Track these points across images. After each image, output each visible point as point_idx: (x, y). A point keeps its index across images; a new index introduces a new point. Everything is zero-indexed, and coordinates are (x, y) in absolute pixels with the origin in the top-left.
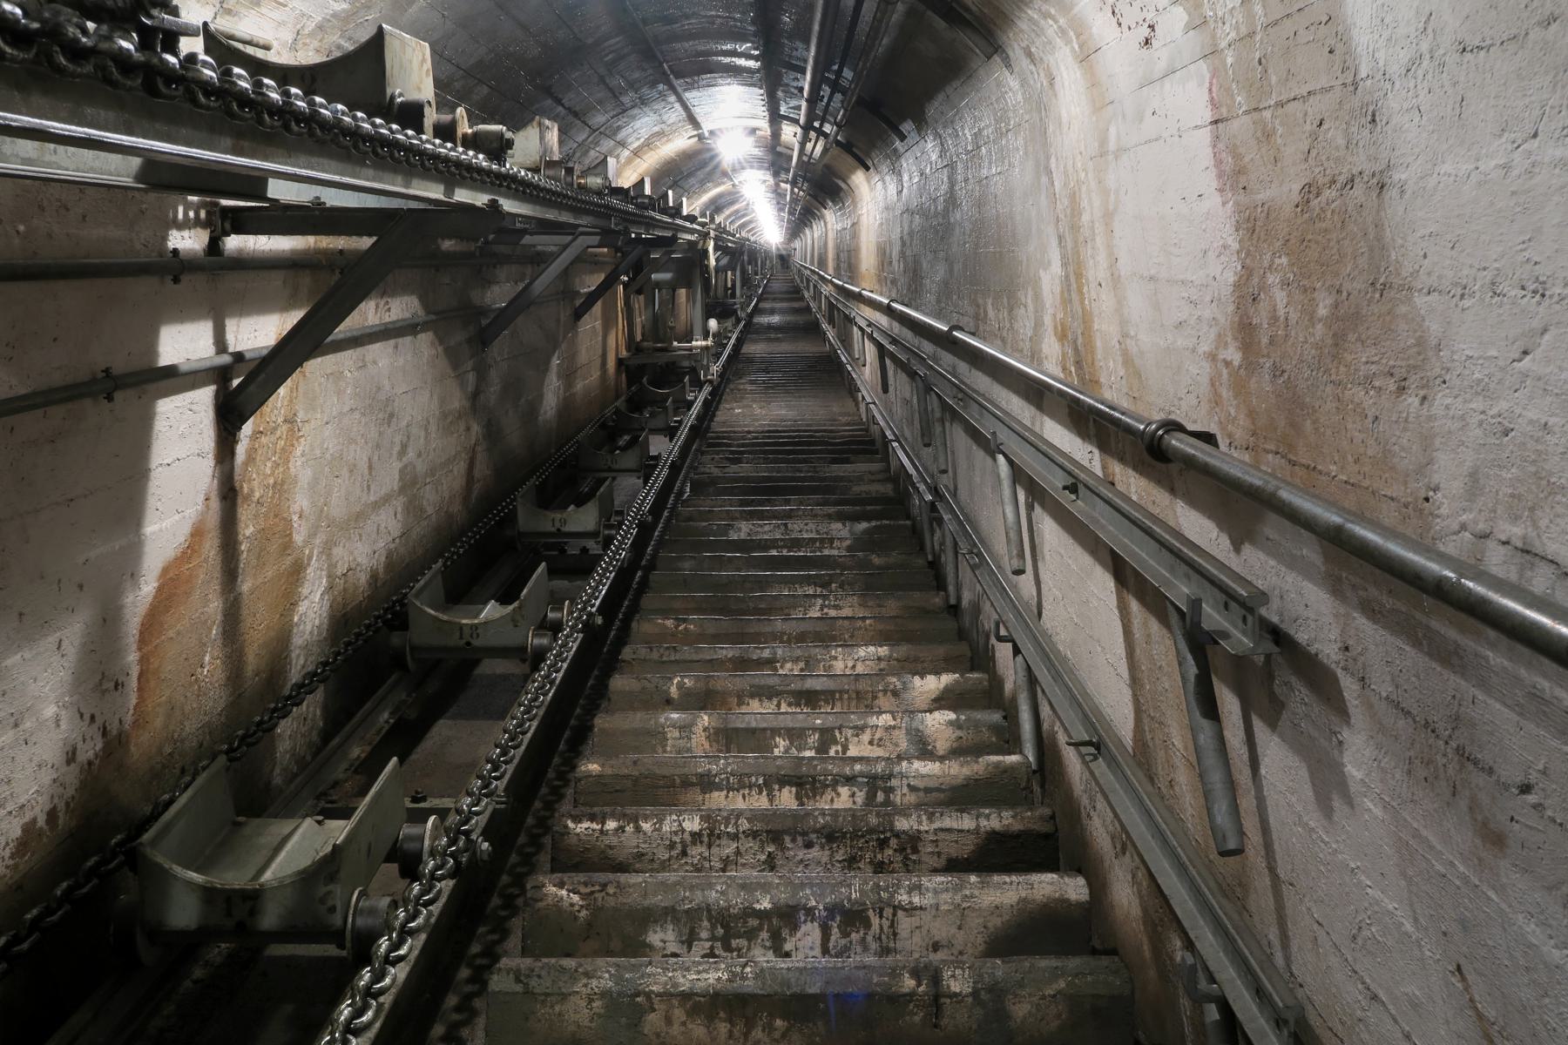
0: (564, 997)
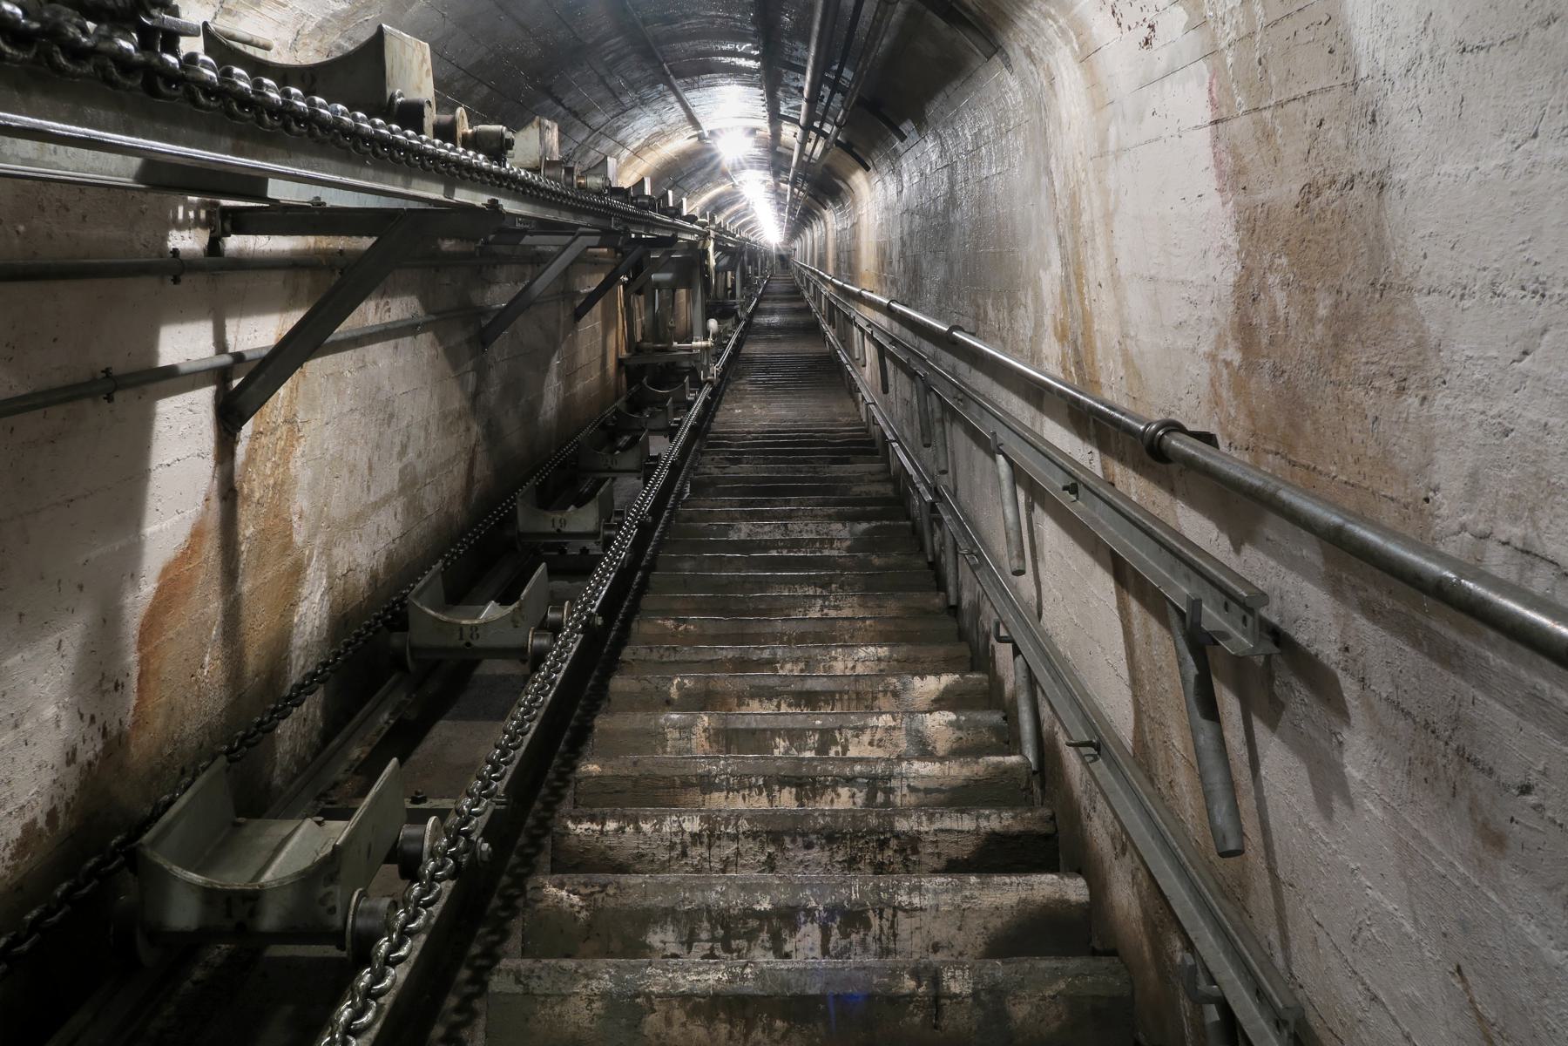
0: (564, 998)
